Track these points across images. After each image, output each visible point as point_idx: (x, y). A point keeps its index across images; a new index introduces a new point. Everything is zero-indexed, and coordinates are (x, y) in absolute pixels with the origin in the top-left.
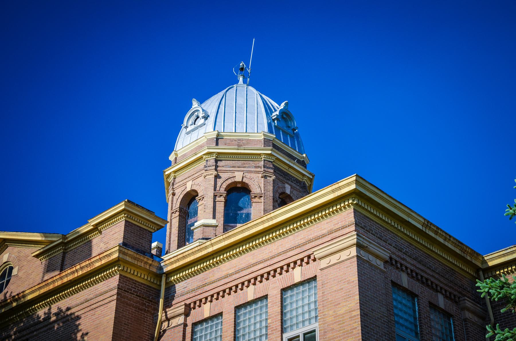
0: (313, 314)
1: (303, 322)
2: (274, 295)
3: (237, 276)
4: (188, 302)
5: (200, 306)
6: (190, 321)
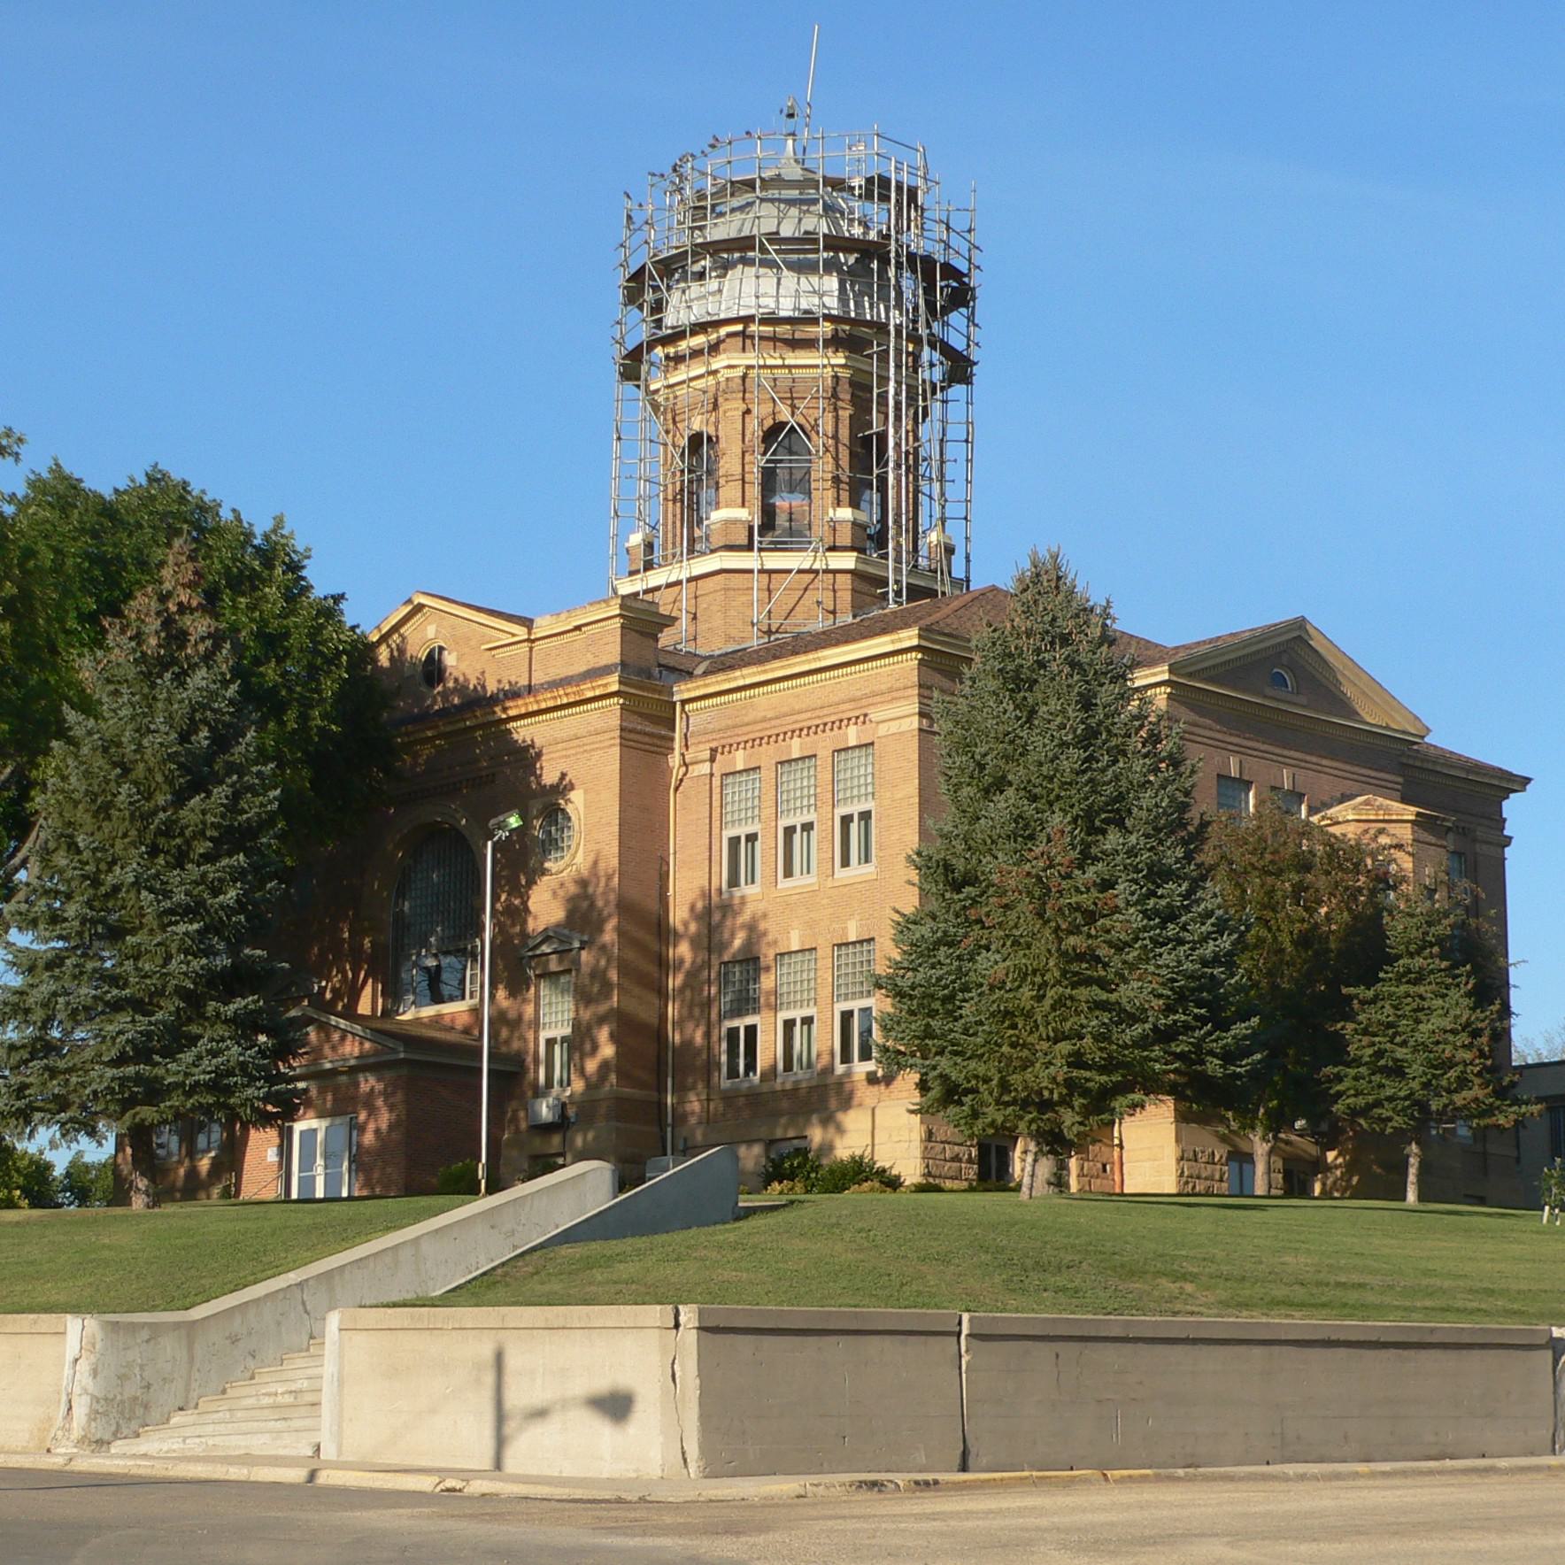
0: (870, 789)
1: (859, 797)
2: (824, 754)
3: (778, 722)
4: (714, 745)
5: (730, 752)
6: (718, 769)
